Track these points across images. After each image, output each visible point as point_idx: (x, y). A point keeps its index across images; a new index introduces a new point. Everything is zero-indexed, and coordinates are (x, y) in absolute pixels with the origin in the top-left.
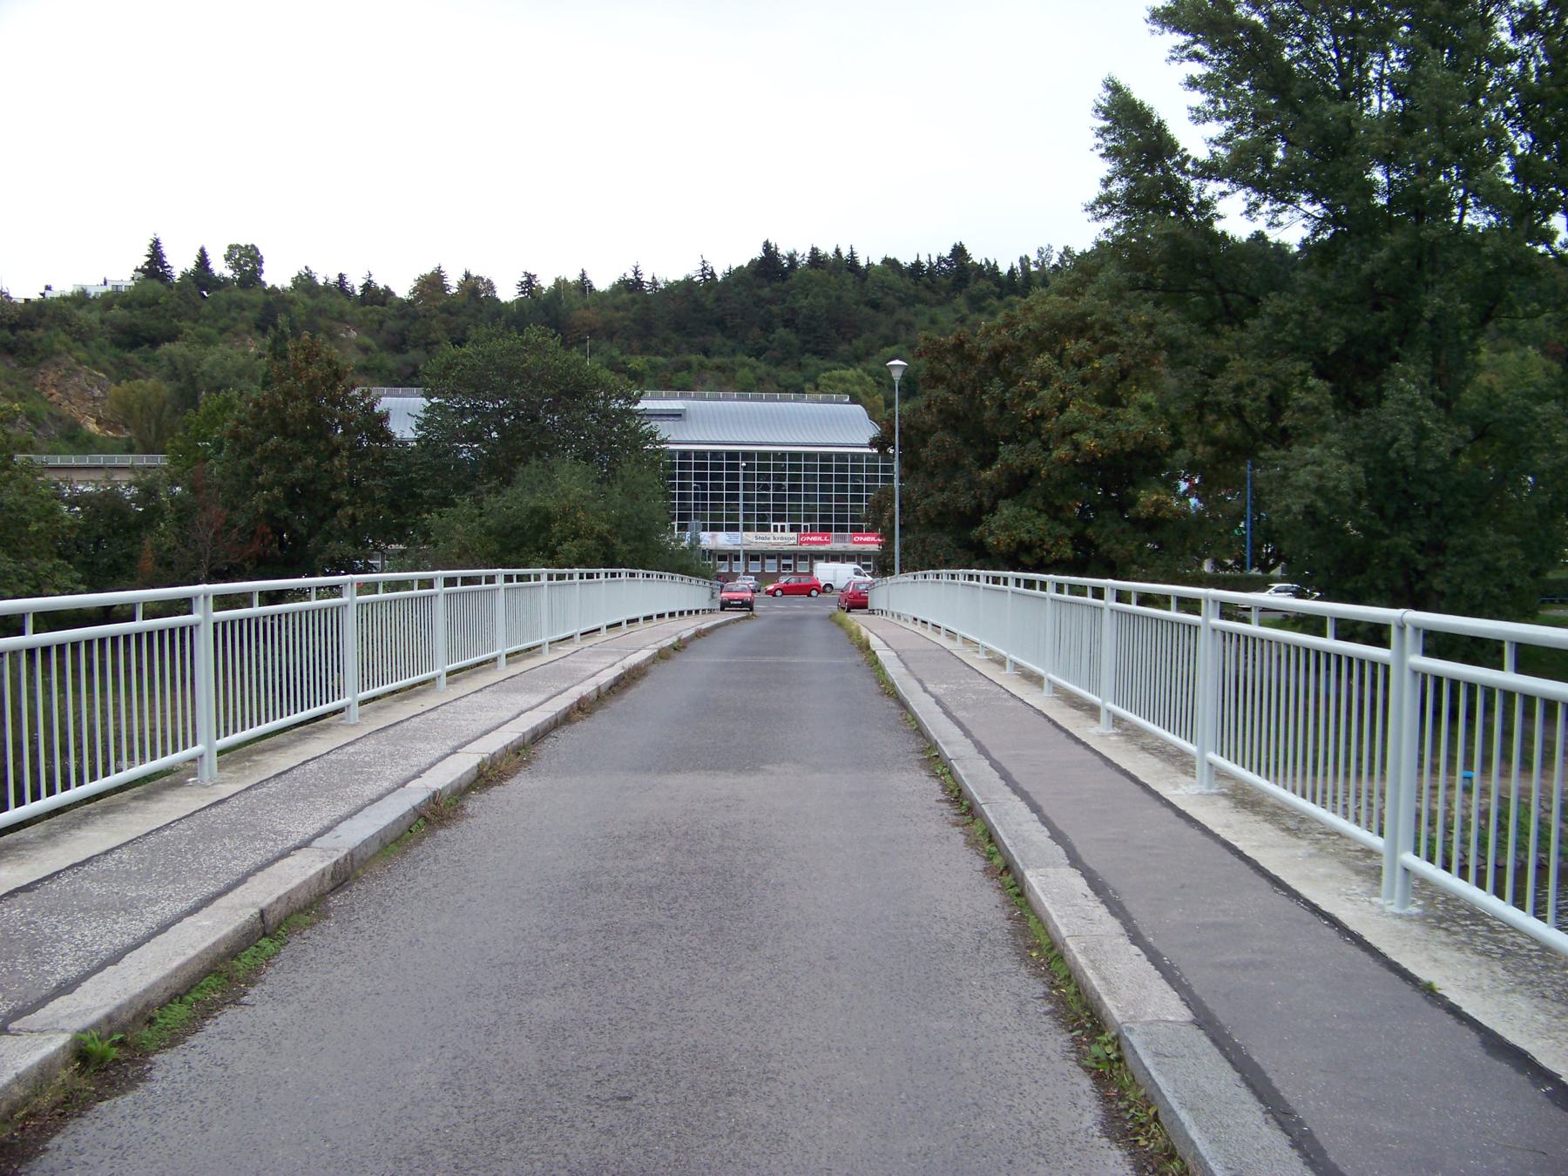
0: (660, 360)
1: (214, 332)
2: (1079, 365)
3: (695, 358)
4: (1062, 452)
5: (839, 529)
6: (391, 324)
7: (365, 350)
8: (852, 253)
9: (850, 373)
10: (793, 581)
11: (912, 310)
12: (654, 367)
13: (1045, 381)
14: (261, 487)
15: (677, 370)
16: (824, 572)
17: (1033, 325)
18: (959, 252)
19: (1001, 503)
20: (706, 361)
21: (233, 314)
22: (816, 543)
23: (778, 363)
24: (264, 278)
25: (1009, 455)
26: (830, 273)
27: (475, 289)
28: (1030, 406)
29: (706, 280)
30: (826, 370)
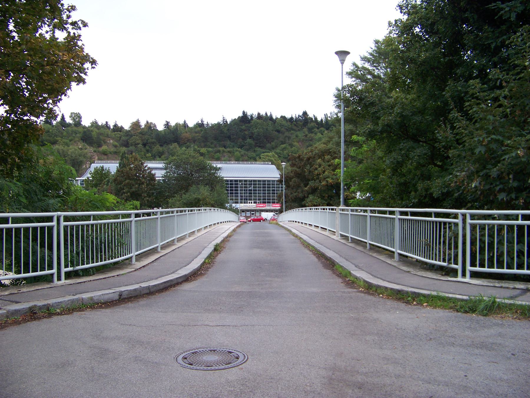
0: (210, 149)
1: (68, 141)
2: (328, 162)
3: (221, 149)
4: (324, 183)
5: (268, 202)
6: (124, 138)
7: (116, 146)
8: (271, 114)
9: (270, 154)
10: (255, 218)
11: (290, 132)
12: (208, 152)
13: (320, 166)
14: (124, 193)
15: (216, 153)
16: (264, 215)
17: (317, 152)
18: (305, 113)
19: (310, 196)
20: (225, 150)
21: (74, 135)
22: (262, 207)
23: (248, 150)
24: (82, 123)
25: (311, 184)
26: (264, 121)
27: (150, 127)
28: (316, 172)
29: (224, 123)
30: (264, 153)
